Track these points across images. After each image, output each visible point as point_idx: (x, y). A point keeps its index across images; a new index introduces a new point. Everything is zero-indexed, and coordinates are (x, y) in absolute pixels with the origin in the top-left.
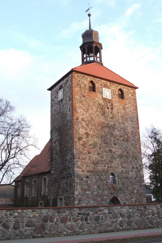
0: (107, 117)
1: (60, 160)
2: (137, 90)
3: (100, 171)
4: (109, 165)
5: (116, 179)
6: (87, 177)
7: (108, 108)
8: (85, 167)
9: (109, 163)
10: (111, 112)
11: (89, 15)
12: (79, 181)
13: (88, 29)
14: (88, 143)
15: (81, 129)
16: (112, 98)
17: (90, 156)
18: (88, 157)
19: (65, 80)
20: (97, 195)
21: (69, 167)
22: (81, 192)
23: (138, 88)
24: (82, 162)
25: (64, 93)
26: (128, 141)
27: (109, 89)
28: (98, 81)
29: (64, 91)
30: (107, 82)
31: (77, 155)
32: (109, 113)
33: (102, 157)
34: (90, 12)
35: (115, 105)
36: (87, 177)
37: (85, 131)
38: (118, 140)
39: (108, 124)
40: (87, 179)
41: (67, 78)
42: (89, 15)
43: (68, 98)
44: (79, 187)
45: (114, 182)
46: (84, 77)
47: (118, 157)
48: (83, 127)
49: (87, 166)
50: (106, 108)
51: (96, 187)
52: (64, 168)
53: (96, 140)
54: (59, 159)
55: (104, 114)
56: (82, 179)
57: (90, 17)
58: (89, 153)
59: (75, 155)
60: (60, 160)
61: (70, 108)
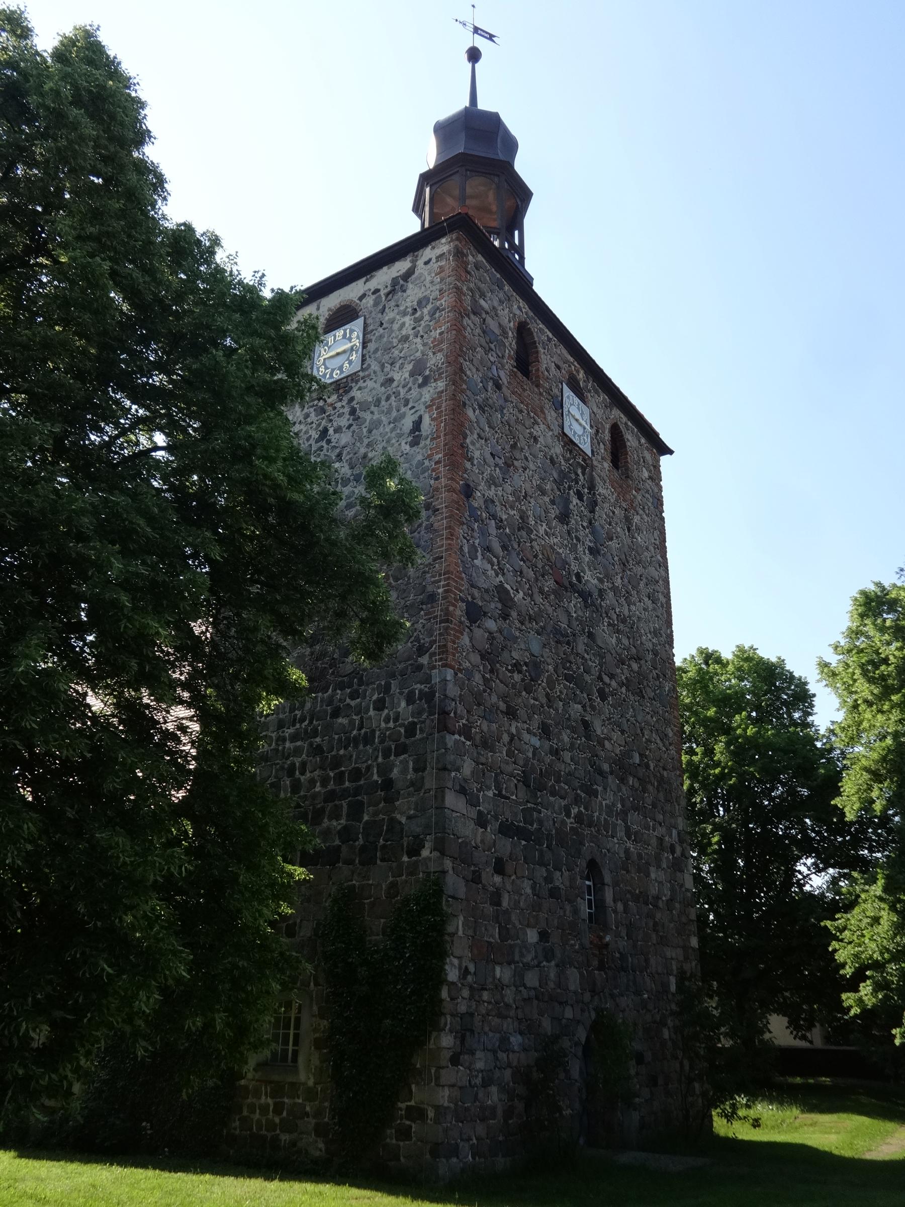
1: (294, 738)
2: (664, 460)
3: (355, 841)
5: (609, 895)
10: (590, 523)
12: (462, 892)
14: (506, 654)
18: (506, 738)
19: (383, 277)
20: (537, 998)
21: (388, 784)
22: (472, 968)
23: (671, 452)
24: (483, 760)
25: (371, 346)
26: (644, 697)
28: (549, 340)
29: (365, 332)
31: (461, 709)
33: (555, 752)
35: (601, 490)
41: (402, 266)
44: (460, 933)
45: (599, 916)
47: (612, 773)
48: (488, 549)
49: (500, 795)
50: (571, 492)
51: (532, 936)
52: (331, 786)
53: (535, 648)
54: (289, 732)
55: (564, 517)
56: (476, 878)
57: (476, 65)
58: (511, 713)
60: (294, 738)
61: (417, 425)
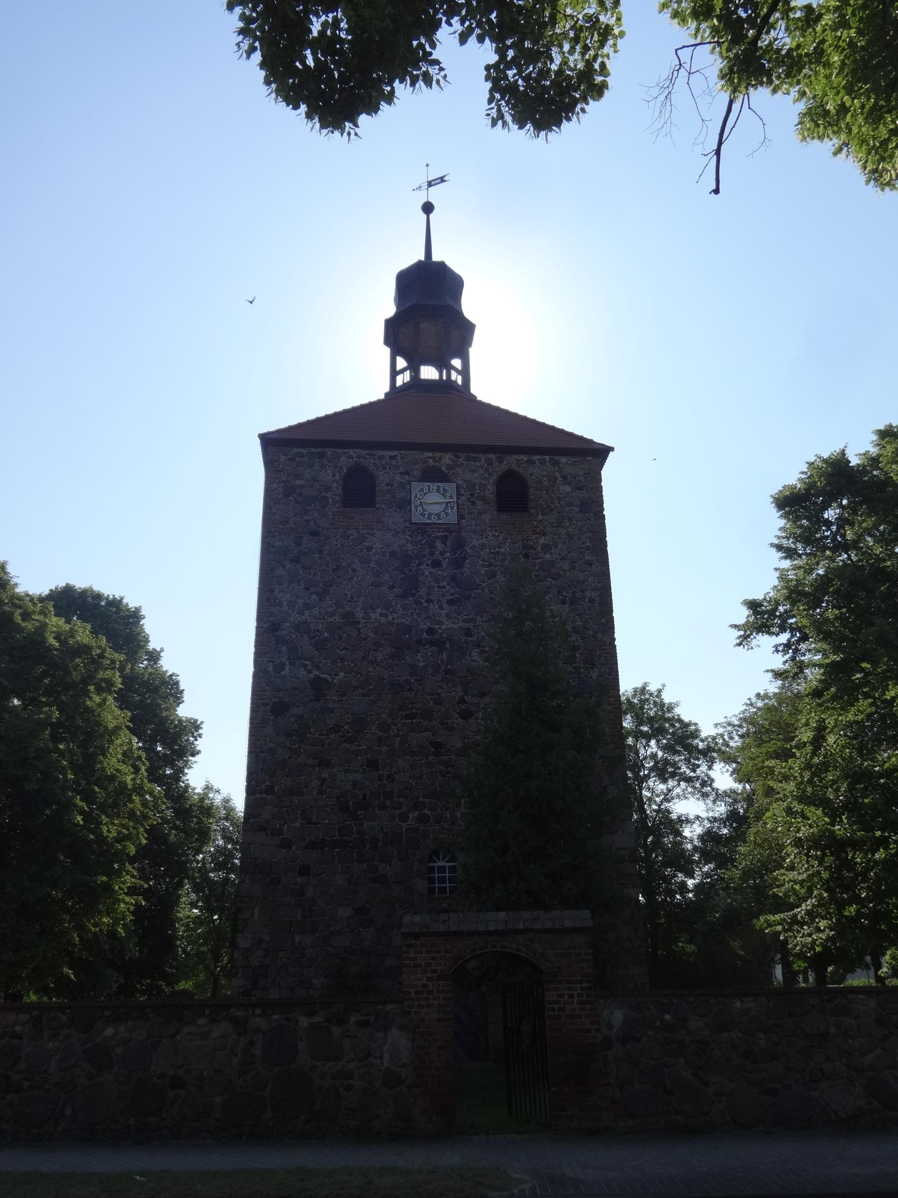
0: (428, 601)
4: (426, 811)
6: (304, 871)
7: (436, 564)
8: (298, 824)
9: (427, 801)
11: (428, 208)
13: (423, 258)
15: (287, 667)
16: (461, 517)
17: (325, 775)
27: (448, 480)
28: (392, 458)
30: (437, 454)
32: (443, 584)
34: (435, 195)
35: (475, 543)
36: (304, 871)
37: (310, 672)
38: (483, 695)
39: (431, 631)
40: (300, 880)
42: (428, 208)
43: (335, 566)
46: (322, 456)
51: (344, 912)
59: (115, 726)
